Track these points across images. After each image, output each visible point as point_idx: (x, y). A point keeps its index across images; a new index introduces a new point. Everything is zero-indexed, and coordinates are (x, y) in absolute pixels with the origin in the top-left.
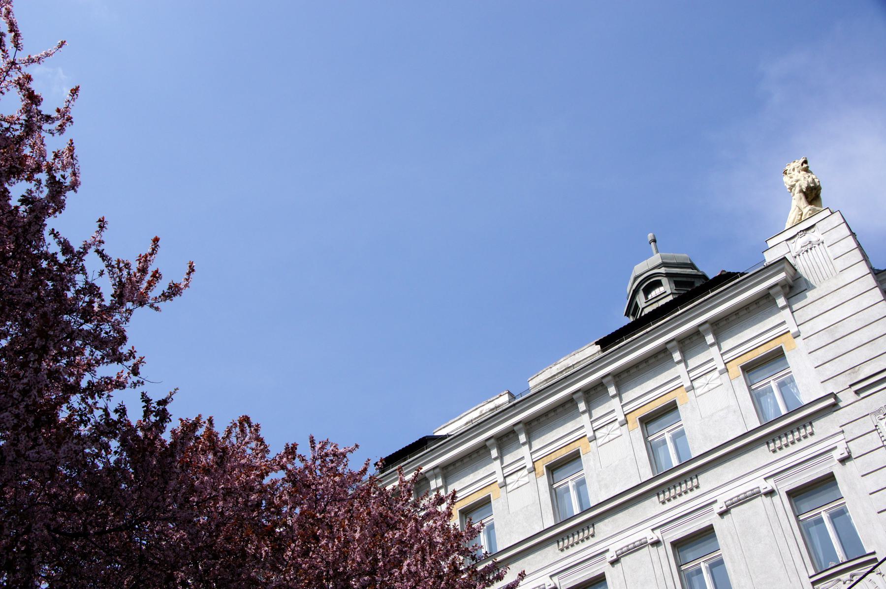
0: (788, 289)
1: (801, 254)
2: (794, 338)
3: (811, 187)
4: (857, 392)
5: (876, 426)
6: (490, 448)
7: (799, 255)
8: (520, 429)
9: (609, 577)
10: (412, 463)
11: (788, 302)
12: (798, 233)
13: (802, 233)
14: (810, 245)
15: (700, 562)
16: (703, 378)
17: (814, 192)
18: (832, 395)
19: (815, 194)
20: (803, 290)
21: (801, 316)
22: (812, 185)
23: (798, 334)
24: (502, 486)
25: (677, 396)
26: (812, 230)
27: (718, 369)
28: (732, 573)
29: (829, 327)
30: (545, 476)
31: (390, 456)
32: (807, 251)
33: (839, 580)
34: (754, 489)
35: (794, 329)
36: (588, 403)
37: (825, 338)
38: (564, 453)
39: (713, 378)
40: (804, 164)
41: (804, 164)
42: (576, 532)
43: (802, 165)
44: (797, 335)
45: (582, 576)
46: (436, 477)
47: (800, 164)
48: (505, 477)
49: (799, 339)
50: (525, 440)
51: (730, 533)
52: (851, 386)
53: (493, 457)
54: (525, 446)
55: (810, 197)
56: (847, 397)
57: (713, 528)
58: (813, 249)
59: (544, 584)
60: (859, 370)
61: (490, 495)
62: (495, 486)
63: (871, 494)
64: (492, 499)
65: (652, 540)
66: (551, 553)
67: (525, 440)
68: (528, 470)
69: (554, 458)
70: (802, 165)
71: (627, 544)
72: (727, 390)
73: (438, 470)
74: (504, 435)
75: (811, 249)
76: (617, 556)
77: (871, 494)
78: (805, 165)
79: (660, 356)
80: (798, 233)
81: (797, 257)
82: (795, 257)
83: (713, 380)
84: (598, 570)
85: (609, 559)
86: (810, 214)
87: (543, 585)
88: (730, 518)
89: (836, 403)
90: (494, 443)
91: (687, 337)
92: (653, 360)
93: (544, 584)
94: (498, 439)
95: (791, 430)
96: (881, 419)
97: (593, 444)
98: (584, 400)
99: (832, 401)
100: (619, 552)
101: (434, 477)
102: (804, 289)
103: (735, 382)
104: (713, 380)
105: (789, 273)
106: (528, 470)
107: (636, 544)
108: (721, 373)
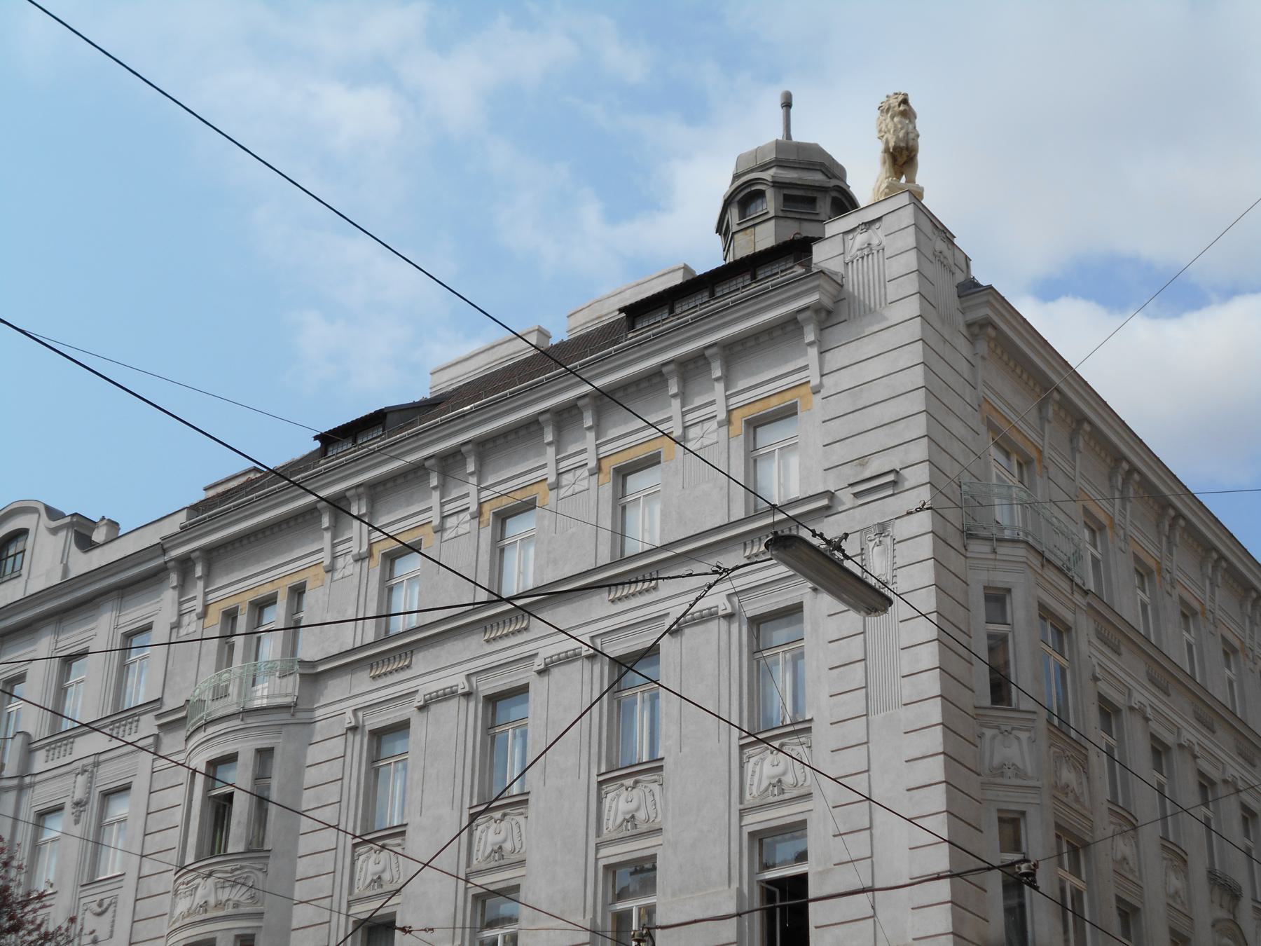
0: (823, 315)
1: (855, 261)
2: (814, 393)
3: (900, 147)
4: (856, 495)
5: (862, 549)
6: (710, 360)
7: (853, 262)
8: (469, 451)
9: (533, 693)
10: (314, 480)
11: (820, 335)
12: (859, 225)
13: (863, 227)
14: (868, 249)
15: (507, 728)
16: (572, 474)
17: (905, 153)
18: (830, 495)
19: (908, 156)
20: (841, 321)
21: (836, 358)
22: (902, 144)
23: (818, 390)
24: (553, 487)
25: (540, 492)
26: (877, 225)
27: (353, 553)
28: (664, 715)
29: (855, 387)
30: (490, 528)
31: (712, 272)
32: (863, 258)
33: (622, 785)
34: (712, 608)
35: (815, 381)
36: (728, 366)
37: (844, 404)
38: (775, 404)
39: (582, 477)
40: (902, 105)
41: (902, 105)
42: (757, 539)
43: (899, 105)
44: (816, 391)
45: (503, 682)
46: (359, 497)
47: (897, 104)
48: (559, 475)
49: (819, 396)
50: (591, 424)
51: (674, 663)
52: (851, 485)
53: (807, 341)
54: (813, 349)
55: (899, 159)
56: (846, 497)
57: (802, 607)
58: (870, 256)
59: (457, 686)
60: (867, 462)
61: (421, 539)
62: (428, 529)
63: (830, 642)
64: (278, 600)
65: (350, 725)
66: (362, 682)
67: (591, 424)
68: (589, 470)
69: (506, 502)
70: (899, 105)
71: (709, 606)
72: (721, 453)
73: (361, 490)
74: (410, 471)
75: (868, 255)
76: (426, 701)
77: (830, 642)
78: (902, 108)
79: (644, 385)
80: (858, 227)
81: (850, 264)
82: (847, 264)
83: (709, 433)
84: (523, 678)
85: (417, 704)
86: (886, 194)
87: (455, 686)
88: (679, 641)
89: (830, 505)
90: (717, 354)
91: (691, 360)
92: (633, 389)
93: (717, 607)
94: (442, 458)
95: (782, 529)
96: (871, 541)
97: (553, 494)
98: (475, 456)
99: (825, 502)
100: (427, 697)
101: (357, 498)
102: (843, 319)
103: (734, 443)
104: (709, 433)
105: (828, 292)
106: (589, 470)
107: (569, 653)
108: (720, 425)
